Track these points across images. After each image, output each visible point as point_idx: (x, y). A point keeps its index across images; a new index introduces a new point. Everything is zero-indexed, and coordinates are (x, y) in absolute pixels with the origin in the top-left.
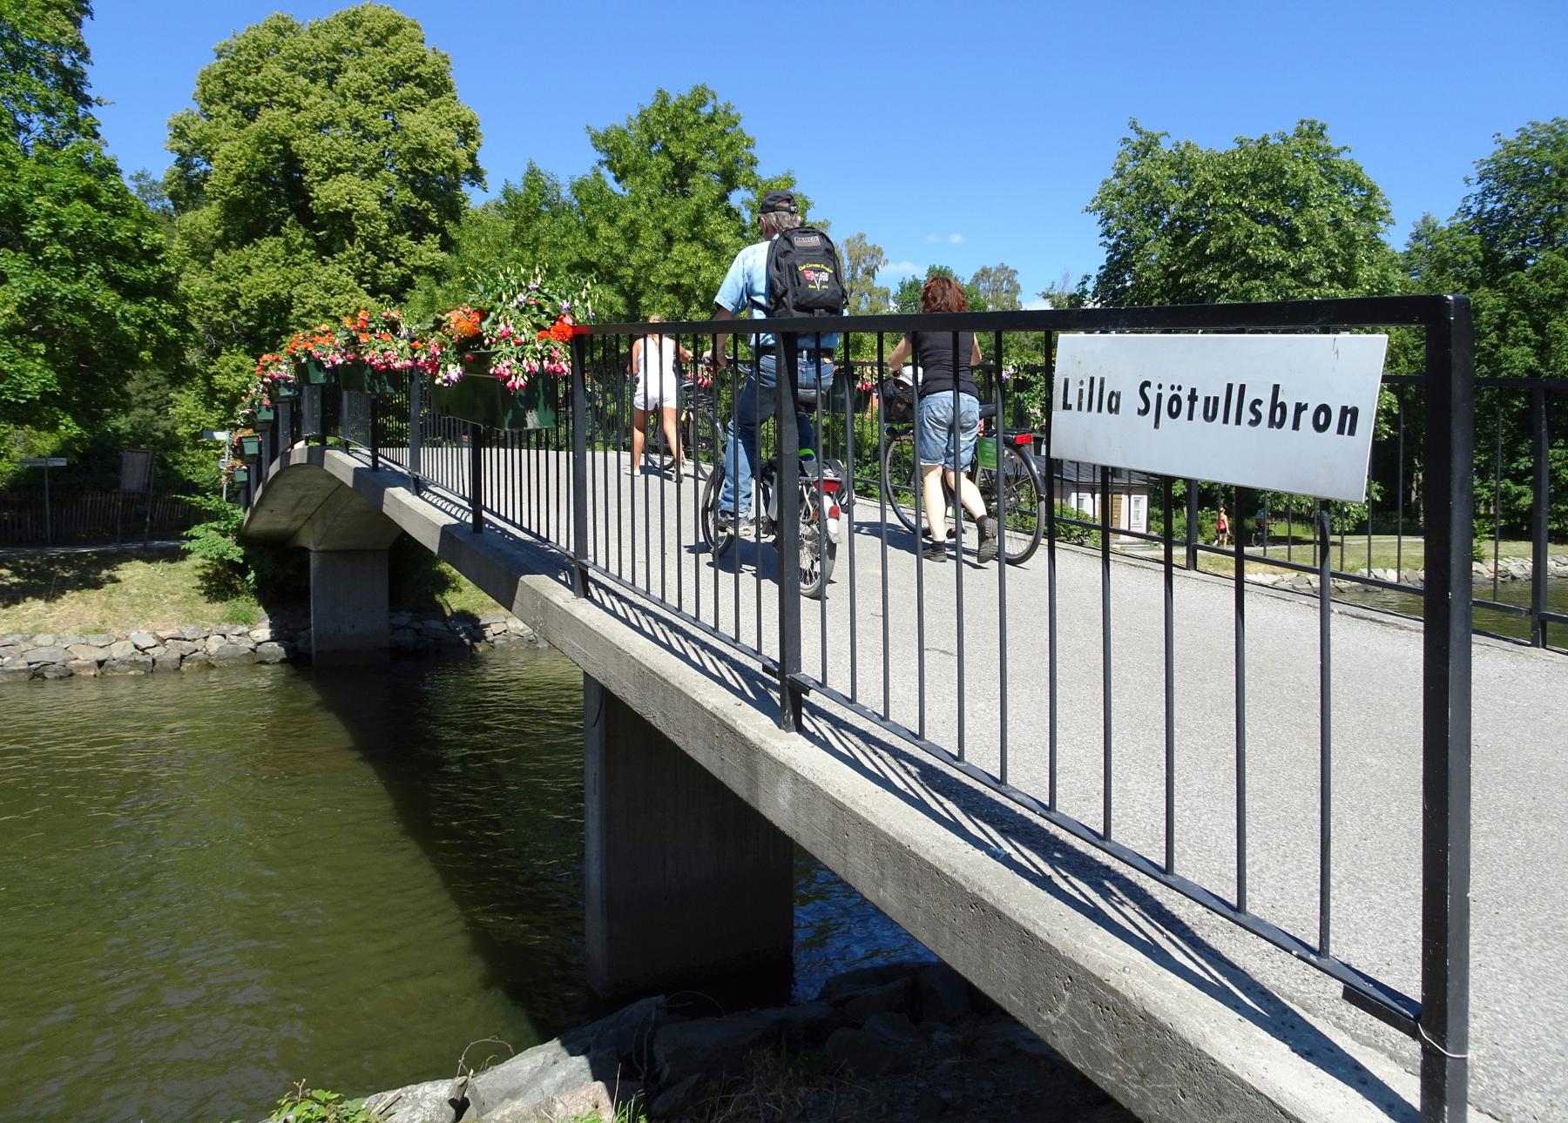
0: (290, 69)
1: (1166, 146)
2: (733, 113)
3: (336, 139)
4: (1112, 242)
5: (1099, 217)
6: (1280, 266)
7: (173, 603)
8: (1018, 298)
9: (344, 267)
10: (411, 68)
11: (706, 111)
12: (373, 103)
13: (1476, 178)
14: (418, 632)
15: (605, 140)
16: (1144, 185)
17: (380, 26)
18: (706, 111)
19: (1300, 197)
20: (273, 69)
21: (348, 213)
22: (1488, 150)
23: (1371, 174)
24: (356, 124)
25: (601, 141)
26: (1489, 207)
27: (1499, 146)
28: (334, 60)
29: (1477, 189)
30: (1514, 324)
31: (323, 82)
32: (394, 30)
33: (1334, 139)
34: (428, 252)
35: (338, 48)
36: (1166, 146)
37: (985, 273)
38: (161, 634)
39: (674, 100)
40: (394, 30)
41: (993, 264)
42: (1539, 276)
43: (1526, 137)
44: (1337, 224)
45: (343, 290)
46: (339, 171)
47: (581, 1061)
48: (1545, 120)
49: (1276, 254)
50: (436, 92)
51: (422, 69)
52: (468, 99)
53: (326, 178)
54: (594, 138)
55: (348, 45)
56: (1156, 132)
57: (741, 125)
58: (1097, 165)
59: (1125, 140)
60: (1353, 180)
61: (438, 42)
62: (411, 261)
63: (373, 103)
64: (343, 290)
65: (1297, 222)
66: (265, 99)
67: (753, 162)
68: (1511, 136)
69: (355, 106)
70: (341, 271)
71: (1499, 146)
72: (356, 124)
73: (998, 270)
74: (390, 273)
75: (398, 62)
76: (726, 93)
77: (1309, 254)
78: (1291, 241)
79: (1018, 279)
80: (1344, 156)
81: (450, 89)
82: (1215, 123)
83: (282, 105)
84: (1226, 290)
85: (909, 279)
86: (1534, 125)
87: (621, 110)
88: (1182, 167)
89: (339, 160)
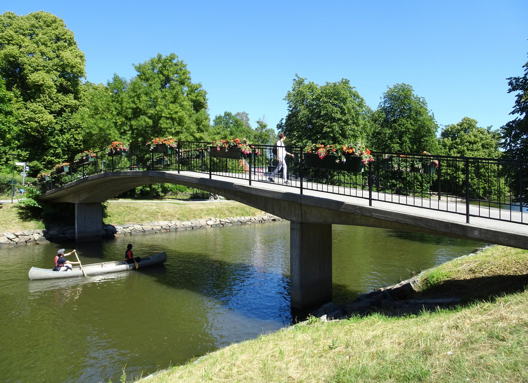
0: (16, 32)
1: (306, 82)
2: (184, 63)
3: (37, 59)
4: (291, 109)
5: (287, 102)
6: (340, 119)
7: (16, 223)
8: (249, 122)
9: (40, 104)
10: (63, 36)
11: (175, 62)
12: (49, 47)
13: (383, 97)
14: (106, 230)
15: (139, 68)
16: (300, 94)
17: (49, 20)
18: (175, 62)
19: (344, 101)
20: (10, 32)
21: (42, 85)
22: (386, 90)
23: (361, 95)
24: (43, 54)
25: (138, 69)
26: (386, 105)
27: (388, 89)
28: (32, 30)
29: (383, 100)
30: (394, 138)
31: (29, 38)
32: (55, 21)
33: (351, 84)
34: (70, 100)
35: (33, 26)
36: (306, 82)
37: (238, 114)
38: (17, 234)
39: (164, 57)
40: (55, 21)
41: (241, 111)
42: (399, 125)
43: (395, 87)
44: (353, 108)
45: (41, 112)
46: (38, 70)
47: (324, 317)
48: (400, 83)
49: (339, 116)
50: (70, 44)
51: (66, 36)
52: (81, 47)
53: (33, 72)
54: (136, 67)
55: (37, 25)
56: (304, 78)
57: (187, 67)
58: (289, 87)
59: (295, 80)
60: (356, 96)
61: (71, 27)
62: (64, 103)
63: (49, 47)
64: (41, 112)
65: (344, 107)
66: (6, 42)
67: (189, 79)
68: (392, 87)
69: (42, 47)
70: (39, 105)
71: (388, 89)
72: (43, 54)
73: (243, 113)
74: (57, 107)
75: (57, 33)
76: (181, 57)
77: (347, 116)
78: (343, 113)
79: (249, 116)
80: (354, 89)
81: (75, 44)
82: (321, 78)
83: (13, 45)
84: (326, 125)
85: (218, 115)
86: (398, 84)
87: (144, 58)
88: (311, 88)
89: (38, 66)
